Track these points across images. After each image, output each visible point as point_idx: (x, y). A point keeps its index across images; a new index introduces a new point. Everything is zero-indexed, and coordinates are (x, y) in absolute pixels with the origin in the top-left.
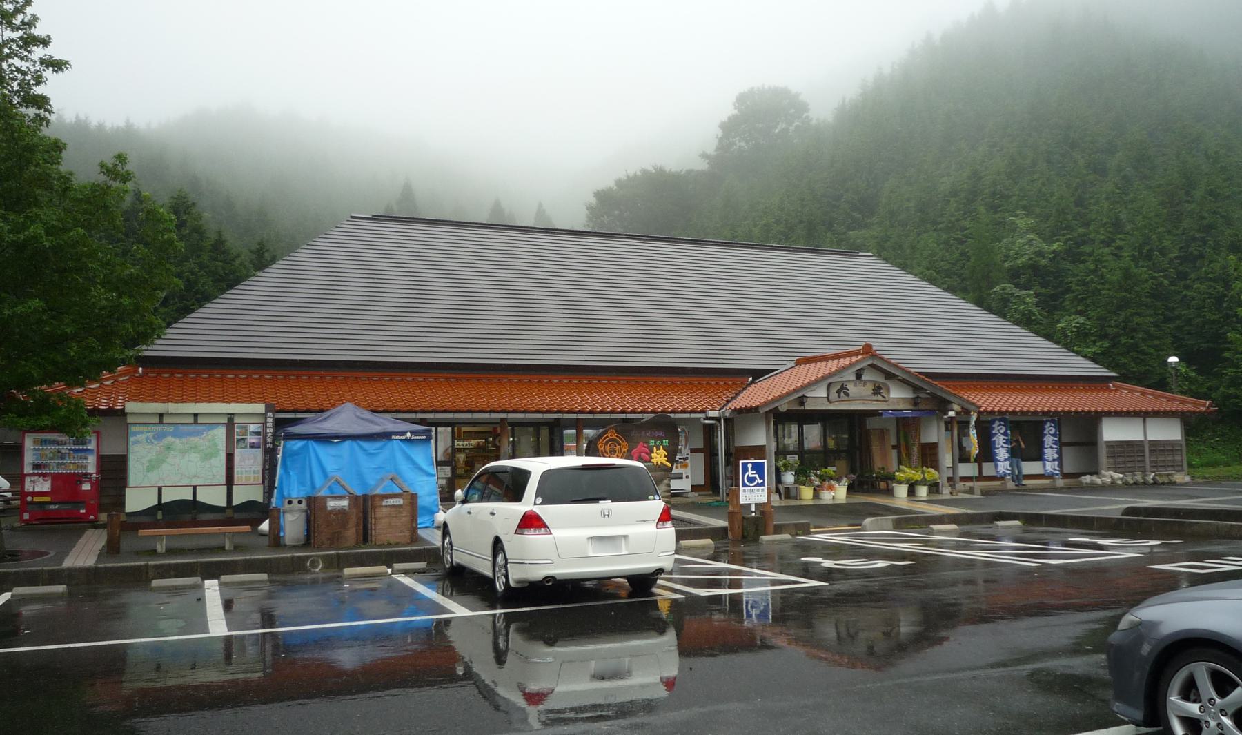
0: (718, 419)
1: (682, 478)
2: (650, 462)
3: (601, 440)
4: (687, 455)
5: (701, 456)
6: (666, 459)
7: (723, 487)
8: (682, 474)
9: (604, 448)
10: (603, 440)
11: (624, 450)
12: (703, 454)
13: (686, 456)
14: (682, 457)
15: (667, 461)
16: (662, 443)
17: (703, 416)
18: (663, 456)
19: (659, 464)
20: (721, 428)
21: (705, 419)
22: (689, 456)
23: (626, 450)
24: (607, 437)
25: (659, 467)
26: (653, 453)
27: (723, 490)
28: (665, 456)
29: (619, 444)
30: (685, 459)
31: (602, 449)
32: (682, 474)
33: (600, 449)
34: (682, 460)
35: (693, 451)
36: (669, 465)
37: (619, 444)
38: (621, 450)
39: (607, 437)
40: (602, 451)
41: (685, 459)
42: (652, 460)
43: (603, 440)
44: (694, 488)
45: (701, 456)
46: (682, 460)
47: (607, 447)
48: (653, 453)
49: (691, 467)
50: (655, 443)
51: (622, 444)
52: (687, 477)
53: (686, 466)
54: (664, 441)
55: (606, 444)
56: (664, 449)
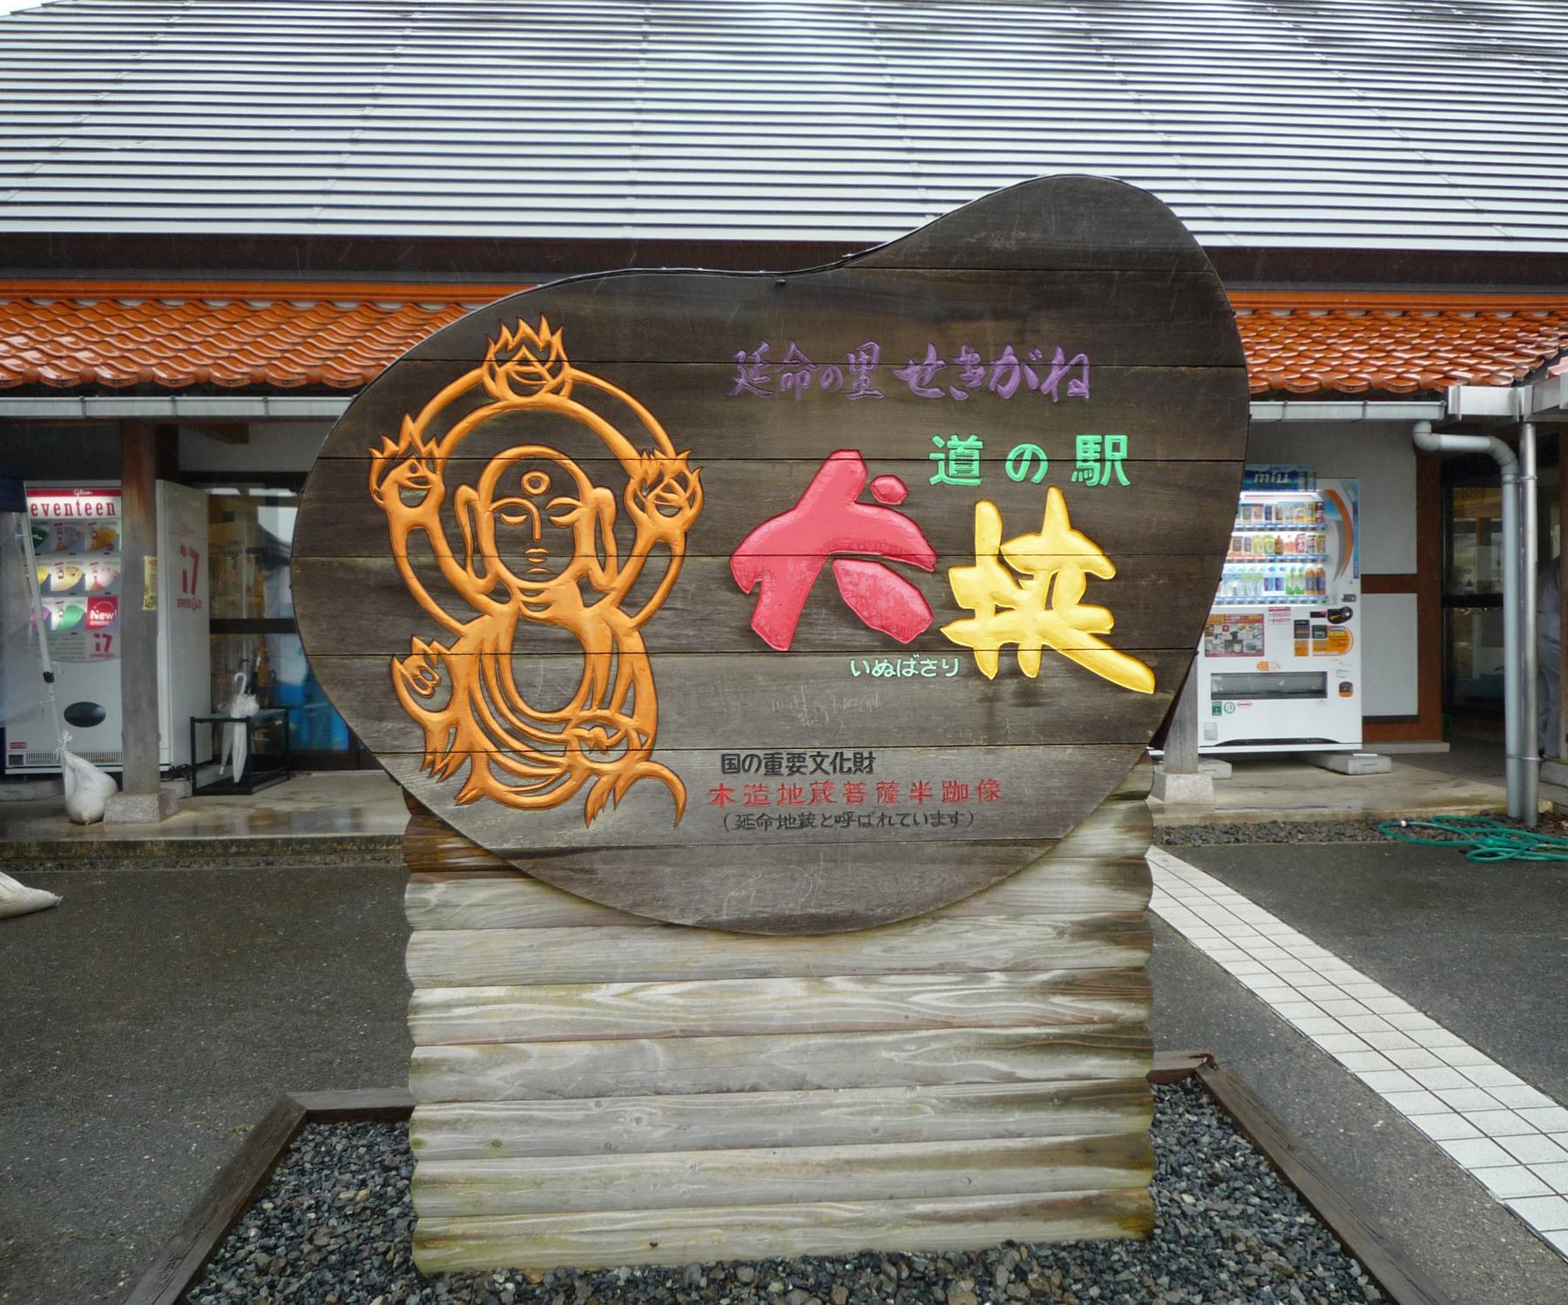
0: (1505, 429)
1: (1321, 693)
2: (933, 643)
3: (412, 428)
4: (1347, 598)
5: (1406, 604)
6: (1102, 618)
7: (1523, 750)
8: (1324, 675)
9: (447, 509)
10: (436, 431)
11: (653, 524)
12: (1414, 596)
13: (1340, 605)
14: (1323, 608)
15: (1114, 640)
16: (1063, 461)
17: (1429, 411)
18: (1072, 585)
19: (1030, 664)
20: (1521, 471)
21: (1440, 427)
22: (1355, 606)
23: (674, 527)
24: (477, 396)
25: (1029, 694)
26: (968, 557)
27: (1523, 764)
28: (1095, 591)
29: (610, 472)
30: (1339, 616)
31: (426, 514)
32: (1324, 675)
33: (402, 515)
34: (1323, 621)
35: (1373, 584)
36: (1135, 675)
37: (610, 472)
38: (624, 520)
39: (477, 396)
40: (418, 534)
41: (1339, 616)
42: (956, 631)
43: (436, 431)
44: (1376, 728)
45: (1406, 604)
46: (1323, 621)
47: (478, 497)
48: (968, 557)
49: (1363, 618)
50: (992, 462)
51: (639, 468)
52: (1345, 689)
53: (1341, 644)
54: (1086, 445)
55: (463, 470)
56: (1077, 523)
